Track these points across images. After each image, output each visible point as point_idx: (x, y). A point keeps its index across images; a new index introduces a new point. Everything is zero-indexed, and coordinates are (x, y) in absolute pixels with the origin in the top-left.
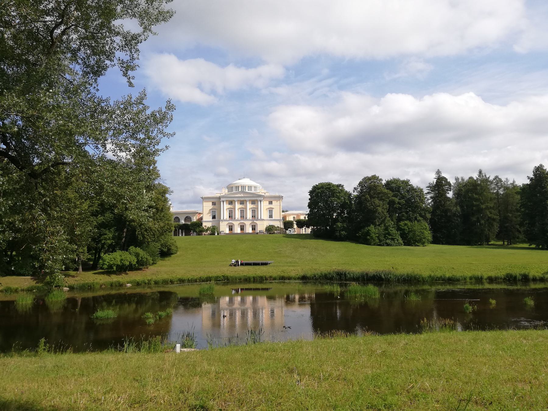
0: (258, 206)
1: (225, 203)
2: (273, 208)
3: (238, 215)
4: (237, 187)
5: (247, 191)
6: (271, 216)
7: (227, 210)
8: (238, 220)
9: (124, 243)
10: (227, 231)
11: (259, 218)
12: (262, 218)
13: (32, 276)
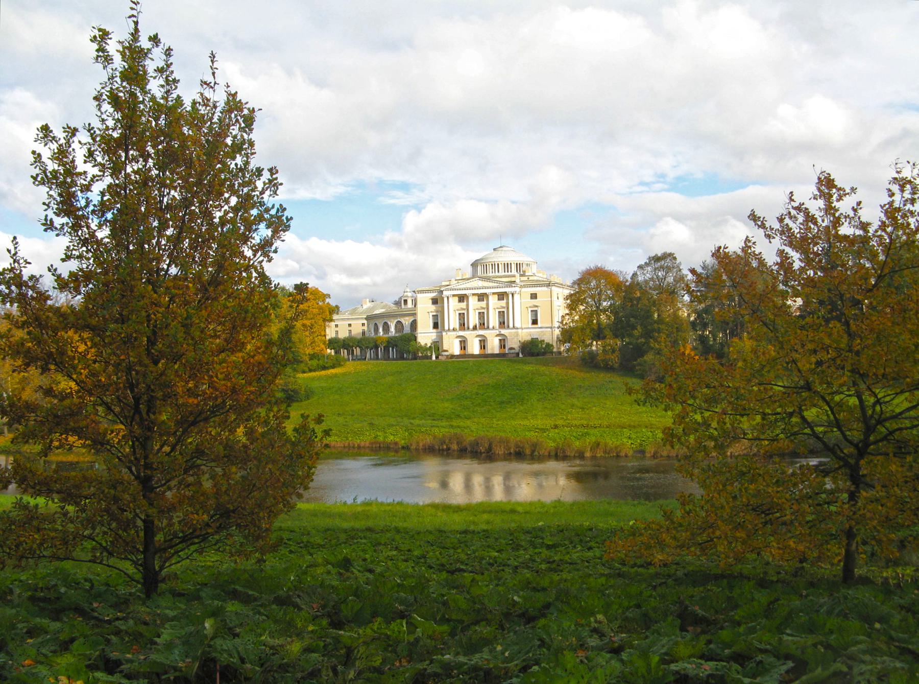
0: (507, 303)
1: (450, 299)
2: (537, 306)
5: (502, 273)
6: (535, 322)
10: (457, 351)
11: (511, 325)
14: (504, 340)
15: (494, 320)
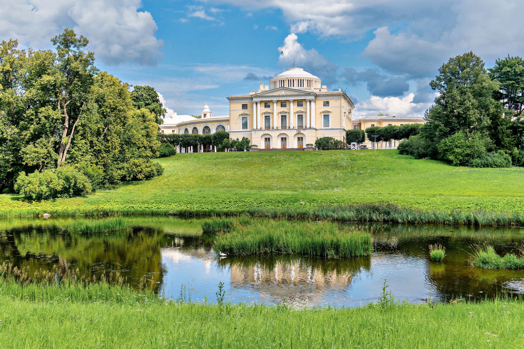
1: (259, 105)
2: (329, 112)
3: (276, 122)
4: (282, 82)
5: (296, 87)
7: (321, 115)
8: (277, 129)
9: (5, 159)
11: (308, 126)
12: (313, 126)
13: (437, 287)
14: (285, 138)
15: (293, 121)
